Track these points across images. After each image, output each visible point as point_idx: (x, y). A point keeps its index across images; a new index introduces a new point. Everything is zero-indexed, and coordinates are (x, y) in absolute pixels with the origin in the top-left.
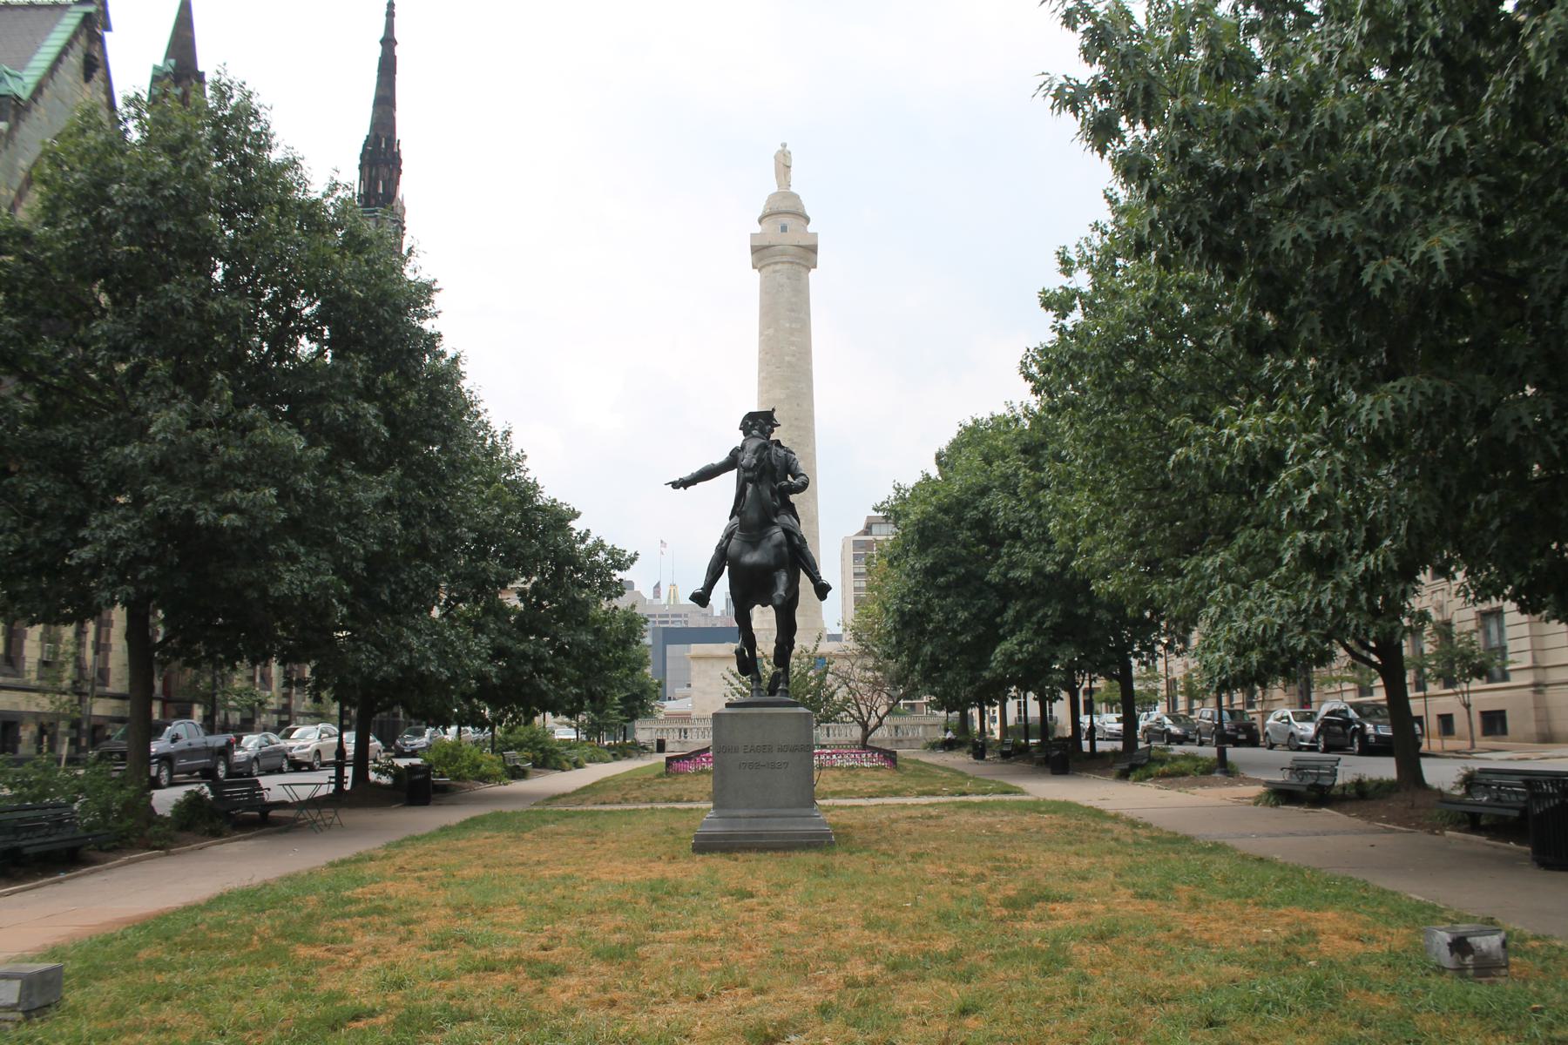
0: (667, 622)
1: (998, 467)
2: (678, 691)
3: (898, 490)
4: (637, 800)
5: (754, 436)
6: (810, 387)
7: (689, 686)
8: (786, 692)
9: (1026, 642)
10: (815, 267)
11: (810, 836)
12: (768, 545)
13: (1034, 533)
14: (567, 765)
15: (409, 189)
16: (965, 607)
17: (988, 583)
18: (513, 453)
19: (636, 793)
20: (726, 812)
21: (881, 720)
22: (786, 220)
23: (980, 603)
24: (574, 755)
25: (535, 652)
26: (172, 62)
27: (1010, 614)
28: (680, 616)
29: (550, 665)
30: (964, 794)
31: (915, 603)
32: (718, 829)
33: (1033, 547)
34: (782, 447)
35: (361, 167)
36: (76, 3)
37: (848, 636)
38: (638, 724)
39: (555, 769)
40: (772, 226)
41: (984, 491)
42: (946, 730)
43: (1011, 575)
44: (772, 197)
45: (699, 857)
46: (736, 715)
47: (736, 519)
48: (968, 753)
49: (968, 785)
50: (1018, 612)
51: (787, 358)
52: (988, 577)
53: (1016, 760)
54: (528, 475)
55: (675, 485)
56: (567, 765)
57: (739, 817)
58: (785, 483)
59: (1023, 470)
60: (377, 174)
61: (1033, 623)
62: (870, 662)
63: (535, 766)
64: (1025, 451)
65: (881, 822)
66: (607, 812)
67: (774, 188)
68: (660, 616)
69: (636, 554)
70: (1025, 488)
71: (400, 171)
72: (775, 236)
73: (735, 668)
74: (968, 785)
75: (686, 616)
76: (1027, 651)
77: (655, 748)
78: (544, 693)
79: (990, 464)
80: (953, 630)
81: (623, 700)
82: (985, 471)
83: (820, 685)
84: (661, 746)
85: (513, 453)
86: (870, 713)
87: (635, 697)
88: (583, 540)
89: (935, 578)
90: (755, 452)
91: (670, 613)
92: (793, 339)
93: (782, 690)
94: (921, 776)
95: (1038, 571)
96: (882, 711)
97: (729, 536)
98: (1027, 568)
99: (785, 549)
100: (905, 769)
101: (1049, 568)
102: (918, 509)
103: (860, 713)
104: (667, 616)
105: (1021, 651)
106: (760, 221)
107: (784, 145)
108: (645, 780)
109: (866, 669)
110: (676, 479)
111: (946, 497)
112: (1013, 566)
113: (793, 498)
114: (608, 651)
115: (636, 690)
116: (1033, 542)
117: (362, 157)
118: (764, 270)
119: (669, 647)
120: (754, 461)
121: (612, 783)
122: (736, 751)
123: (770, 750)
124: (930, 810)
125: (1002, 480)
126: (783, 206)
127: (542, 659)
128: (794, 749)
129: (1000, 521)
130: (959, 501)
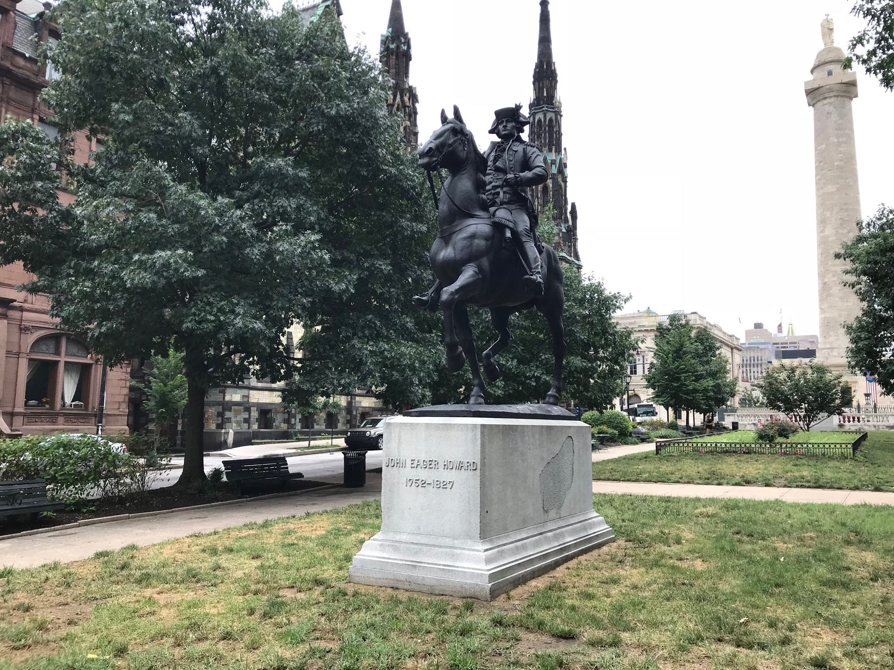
6: (856, 181)
10: (856, 96)
15: (563, 93)
22: (831, 67)
26: (390, 30)
35: (534, 83)
36: (323, 2)
44: (820, 54)
51: (836, 163)
60: (543, 84)
67: (822, 47)
71: (556, 82)
77: (731, 427)
91: (788, 342)
92: (840, 149)
104: (787, 343)
106: (812, 72)
117: (534, 77)
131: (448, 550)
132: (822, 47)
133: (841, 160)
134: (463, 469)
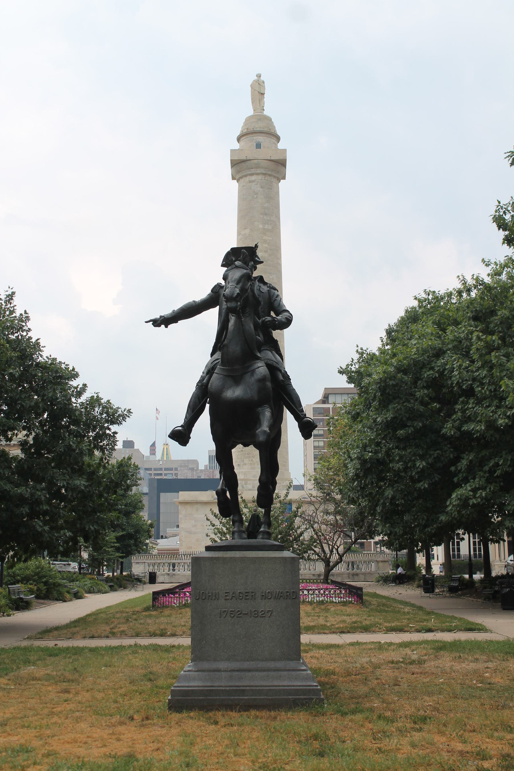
0: (161, 474)
1: (451, 333)
2: (170, 531)
3: (362, 354)
4: (123, 634)
5: (237, 267)
7: (178, 526)
8: (268, 535)
9: (479, 489)
10: (284, 178)
11: (297, 692)
12: (251, 380)
13: (486, 391)
14: (68, 596)
16: (422, 457)
17: (444, 436)
18: (17, 314)
19: (124, 627)
20: (206, 665)
21: (341, 557)
22: (260, 138)
23: (436, 453)
24: (75, 587)
25: (32, 495)
27: (464, 463)
28: (171, 469)
29: (45, 507)
30: (430, 630)
31: (376, 452)
32: (196, 684)
33: (486, 403)
34: (265, 283)
37: (310, 485)
38: (134, 559)
39: (57, 600)
40: (249, 143)
41: (439, 353)
42: (397, 567)
43: (465, 428)
44: (248, 120)
45: (176, 716)
46: (217, 559)
47: (218, 355)
48: (419, 586)
49: (432, 623)
50: (471, 461)
52: (444, 431)
53: (464, 595)
54: (30, 334)
55: (156, 323)
56: (68, 596)
57: (219, 670)
58: (269, 318)
59: (476, 334)
61: (485, 472)
62: (331, 507)
63: (38, 597)
64: (475, 318)
65: (363, 667)
66: (93, 650)
67: (250, 112)
68: (155, 469)
69: (129, 411)
70: (477, 349)
72: (251, 153)
73: (217, 510)
74: (432, 623)
75: (176, 469)
76: (481, 497)
77: (147, 579)
78: (40, 534)
79: (444, 330)
80: (412, 478)
81: (119, 539)
82: (439, 337)
83: (291, 526)
84: (153, 578)
85: (17, 314)
86: (332, 551)
87: (130, 536)
88: (79, 394)
89: (395, 430)
90: (238, 282)
92: (265, 238)
93: (264, 532)
94: (387, 612)
95: (491, 425)
96: (341, 549)
97: (210, 371)
98: (480, 421)
99: (269, 384)
100: (370, 604)
101: (500, 422)
102: (380, 369)
103: (323, 551)
104: (161, 469)
105: (474, 497)
106: (239, 139)
107: (259, 76)
108: (134, 613)
109: (327, 513)
110: (157, 316)
111: (404, 359)
112: (468, 419)
113: (276, 334)
114: (101, 496)
115: (132, 531)
116: (485, 398)
118: (242, 180)
119: (162, 495)
120: (237, 291)
121: (103, 616)
122: (217, 597)
123: (254, 598)
124: (408, 651)
125: (455, 343)
126: (259, 126)
127: (38, 502)
128: (279, 597)
129: (455, 380)
130: (416, 363)
131: (265, 673)
132: (251, 112)
133: (266, 252)
134: (281, 598)
